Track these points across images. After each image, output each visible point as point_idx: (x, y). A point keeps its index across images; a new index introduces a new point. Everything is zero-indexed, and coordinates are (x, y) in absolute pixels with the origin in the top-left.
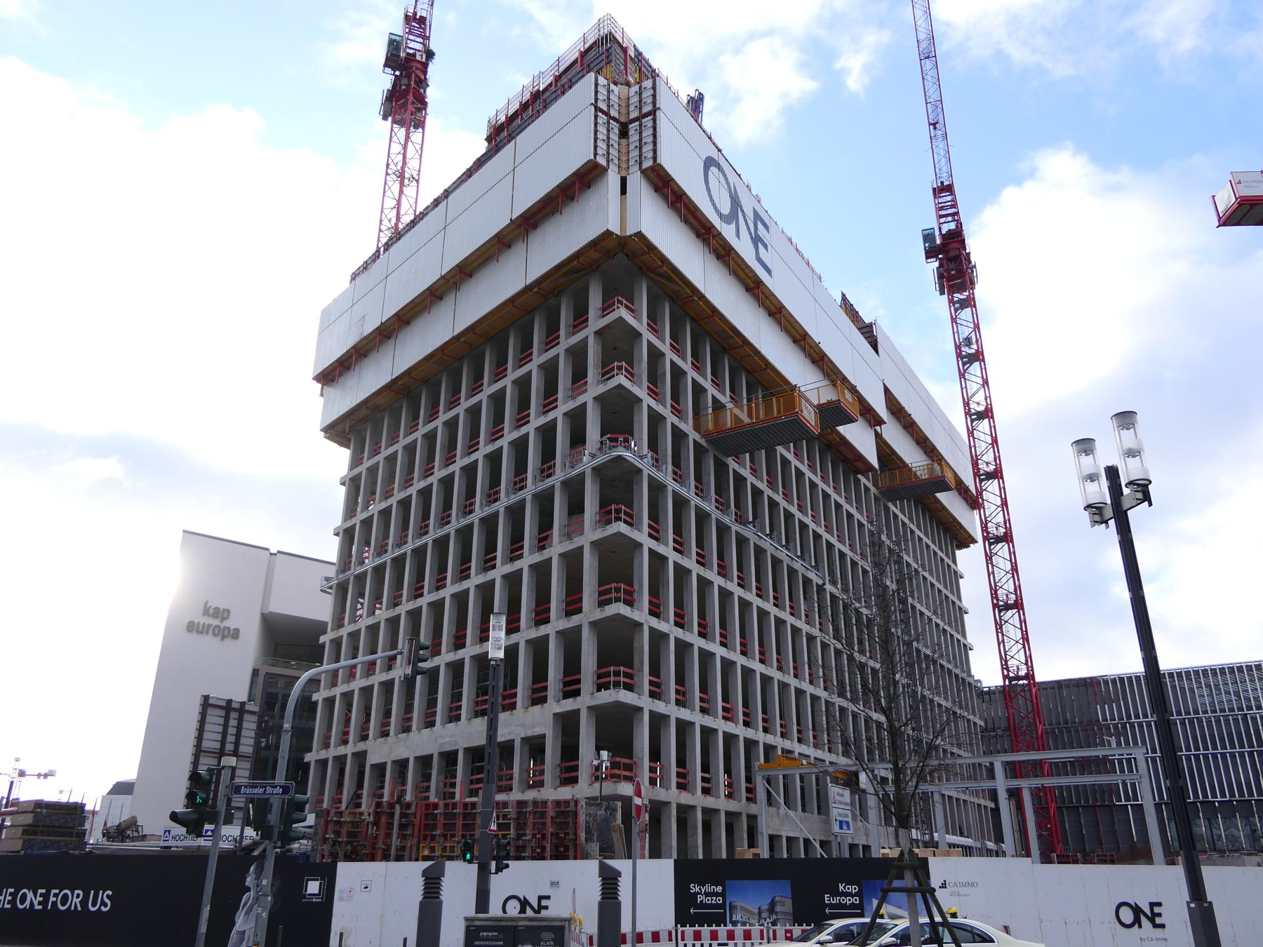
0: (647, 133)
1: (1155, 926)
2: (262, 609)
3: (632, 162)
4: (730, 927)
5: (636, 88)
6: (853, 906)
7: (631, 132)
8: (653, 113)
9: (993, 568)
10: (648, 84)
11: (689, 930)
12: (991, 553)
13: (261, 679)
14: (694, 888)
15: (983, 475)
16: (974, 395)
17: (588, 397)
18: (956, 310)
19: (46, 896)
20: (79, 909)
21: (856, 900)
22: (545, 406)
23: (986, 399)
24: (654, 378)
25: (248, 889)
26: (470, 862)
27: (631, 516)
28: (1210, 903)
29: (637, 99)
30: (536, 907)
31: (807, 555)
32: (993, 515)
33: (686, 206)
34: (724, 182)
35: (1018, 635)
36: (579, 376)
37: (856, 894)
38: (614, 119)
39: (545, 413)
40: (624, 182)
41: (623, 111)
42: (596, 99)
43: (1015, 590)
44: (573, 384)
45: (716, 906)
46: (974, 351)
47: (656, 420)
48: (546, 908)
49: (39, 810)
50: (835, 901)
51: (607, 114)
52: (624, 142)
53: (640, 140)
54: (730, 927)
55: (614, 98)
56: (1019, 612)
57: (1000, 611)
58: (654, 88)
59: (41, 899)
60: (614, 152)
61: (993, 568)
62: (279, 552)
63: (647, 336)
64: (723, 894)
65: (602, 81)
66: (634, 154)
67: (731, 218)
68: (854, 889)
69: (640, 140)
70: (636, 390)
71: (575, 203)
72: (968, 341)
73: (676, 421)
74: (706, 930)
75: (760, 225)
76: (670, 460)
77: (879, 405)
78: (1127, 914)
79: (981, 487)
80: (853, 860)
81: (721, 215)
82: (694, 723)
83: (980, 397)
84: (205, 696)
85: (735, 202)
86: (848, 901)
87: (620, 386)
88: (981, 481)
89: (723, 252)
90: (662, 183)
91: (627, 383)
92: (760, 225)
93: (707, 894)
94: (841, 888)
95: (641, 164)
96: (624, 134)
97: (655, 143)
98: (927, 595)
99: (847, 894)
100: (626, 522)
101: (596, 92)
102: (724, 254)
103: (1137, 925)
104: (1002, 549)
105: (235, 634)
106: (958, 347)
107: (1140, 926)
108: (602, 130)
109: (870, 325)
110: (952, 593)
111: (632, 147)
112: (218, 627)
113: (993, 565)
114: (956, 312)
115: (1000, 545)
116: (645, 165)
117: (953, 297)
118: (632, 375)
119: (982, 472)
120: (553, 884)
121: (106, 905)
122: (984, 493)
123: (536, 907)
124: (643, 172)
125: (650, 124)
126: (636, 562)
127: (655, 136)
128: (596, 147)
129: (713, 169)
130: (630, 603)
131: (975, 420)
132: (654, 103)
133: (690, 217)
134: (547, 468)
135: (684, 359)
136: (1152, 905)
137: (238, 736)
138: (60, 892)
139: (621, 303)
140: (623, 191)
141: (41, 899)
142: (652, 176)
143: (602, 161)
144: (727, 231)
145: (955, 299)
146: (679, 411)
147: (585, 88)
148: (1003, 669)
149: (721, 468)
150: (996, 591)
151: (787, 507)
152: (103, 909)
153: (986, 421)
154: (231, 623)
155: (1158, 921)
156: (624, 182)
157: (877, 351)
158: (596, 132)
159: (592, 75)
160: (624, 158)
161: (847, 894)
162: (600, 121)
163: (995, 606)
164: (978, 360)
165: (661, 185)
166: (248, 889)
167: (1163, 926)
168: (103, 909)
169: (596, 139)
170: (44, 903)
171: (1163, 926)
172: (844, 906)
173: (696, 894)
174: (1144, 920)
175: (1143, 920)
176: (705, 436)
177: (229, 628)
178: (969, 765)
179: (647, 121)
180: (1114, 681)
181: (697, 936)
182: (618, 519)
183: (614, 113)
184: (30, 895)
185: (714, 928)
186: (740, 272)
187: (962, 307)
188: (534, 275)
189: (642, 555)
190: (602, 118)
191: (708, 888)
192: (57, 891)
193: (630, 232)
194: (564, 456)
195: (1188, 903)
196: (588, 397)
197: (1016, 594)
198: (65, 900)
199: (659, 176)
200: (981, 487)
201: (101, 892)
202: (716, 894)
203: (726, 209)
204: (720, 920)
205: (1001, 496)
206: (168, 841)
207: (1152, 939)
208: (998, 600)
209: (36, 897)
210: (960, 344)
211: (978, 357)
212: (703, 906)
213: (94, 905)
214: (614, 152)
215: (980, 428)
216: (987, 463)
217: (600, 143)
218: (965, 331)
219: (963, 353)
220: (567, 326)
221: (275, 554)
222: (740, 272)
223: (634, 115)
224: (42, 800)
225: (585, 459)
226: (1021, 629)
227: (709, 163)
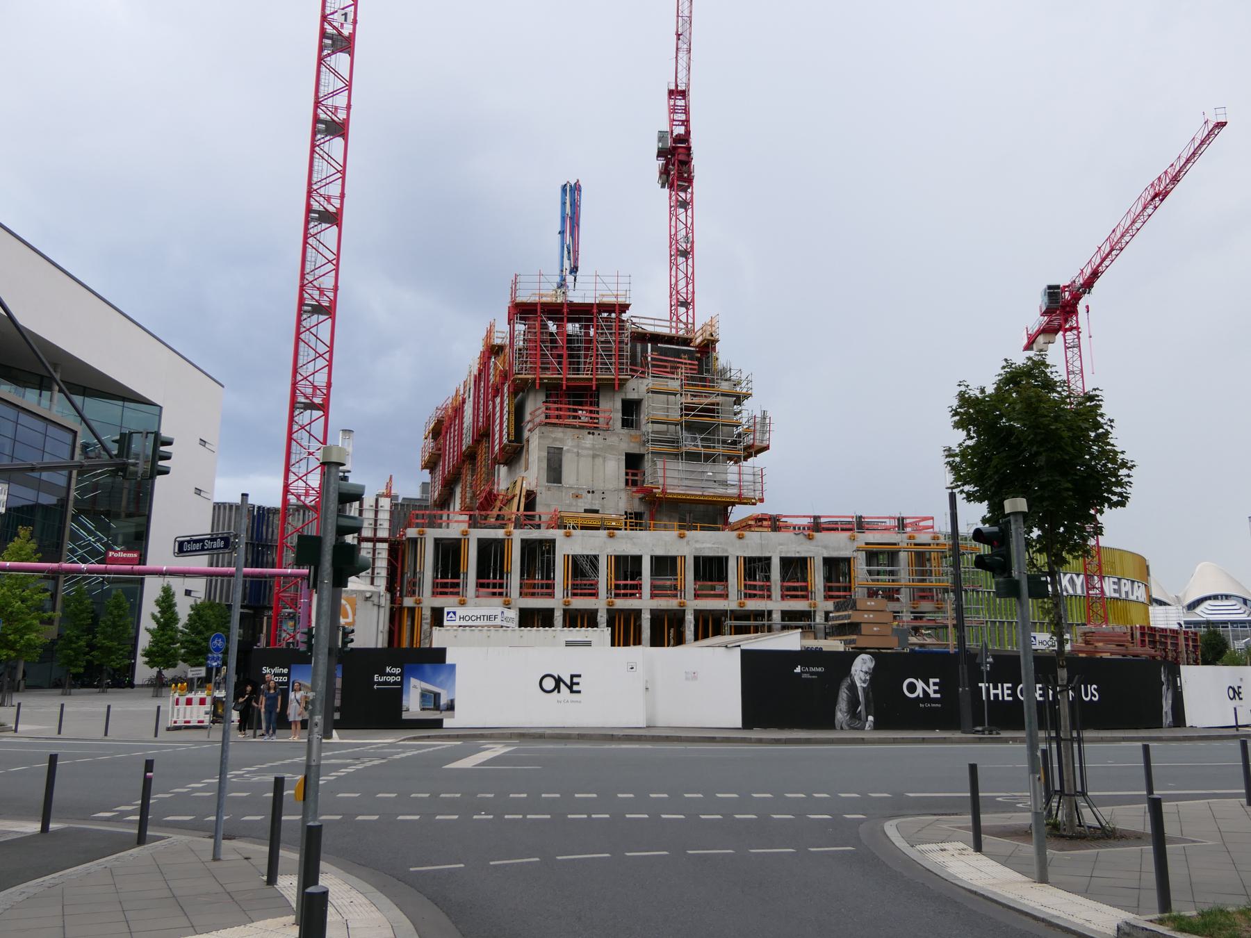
1: (572, 692)
21: (398, 679)
30: (569, 683)
37: (399, 675)
45: (395, 683)
48: (578, 684)
50: (383, 679)
59: (1041, 692)
68: (397, 671)
78: (549, 684)
80: (288, 650)
86: (391, 679)
93: (276, 675)
94: (388, 670)
99: (391, 675)
103: (556, 691)
107: (559, 692)
121: (1095, 697)
123: (569, 683)
141: (1041, 692)
152: (1093, 698)
155: (575, 688)
161: (391, 675)
178: (568, 556)
184: (920, 685)
191: (277, 670)
202: (283, 675)
206: (455, 620)
207: (568, 701)
209: (929, 687)
213: (1087, 696)
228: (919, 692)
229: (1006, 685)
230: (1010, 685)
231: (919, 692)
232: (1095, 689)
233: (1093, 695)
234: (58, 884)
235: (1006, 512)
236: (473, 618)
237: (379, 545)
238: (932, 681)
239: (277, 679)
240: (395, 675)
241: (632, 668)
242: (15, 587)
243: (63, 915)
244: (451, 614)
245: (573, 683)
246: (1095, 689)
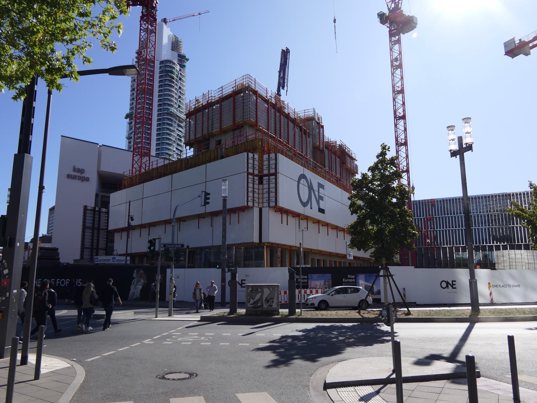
1: (453, 288)
2: (97, 170)
6: (353, 282)
9: (397, 129)
12: (398, 150)
13: (100, 198)
15: (398, 117)
16: (397, 83)
20: (66, 285)
21: (354, 280)
25: (135, 278)
26: (218, 268)
28: (476, 280)
32: (401, 134)
35: (404, 155)
37: (354, 278)
43: (407, 165)
48: (455, 285)
49: (41, 251)
50: (347, 280)
56: (407, 174)
61: (397, 129)
62: (103, 145)
68: (353, 277)
72: (396, 60)
78: (444, 285)
79: (395, 97)
84: (85, 206)
86: (351, 281)
88: (395, 94)
94: (349, 276)
105: (87, 179)
106: (392, 62)
107: (448, 288)
112: (80, 176)
113: (397, 128)
115: (402, 147)
117: (391, 39)
119: (397, 116)
120: (246, 276)
121: (80, 284)
122: (396, 99)
123: (451, 284)
131: (396, 94)
136: (453, 281)
137: (99, 221)
138: (60, 280)
145: (392, 40)
148: (396, 141)
150: (397, 138)
152: (79, 285)
154: (85, 175)
155: (454, 286)
166: (135, 278)
167: (455, 288)
168: (79, 285)
171: (455, 288)
172: (350, 282)
174: (449, 286)
175: (449, 285)
177: (84, 177)
180: (440, 201)
185: (305, 289)
187: (397, 69)
192: (59, 280)
195: (469, 280)
198: (63, 282)
200: (397, 123)
201: (77, 280)
202: (305, 279)
205: (406, 153)
210: (393, 60)
211: (400, 66)
216: (398, 87)
218: (395, 55)
219: (394, 65)
221: (101, 146)
224: (55, 248)
229: (39, 280)
230: (41, 279)
232: (80, 281)
236: (121, 261)
237: (271, 177)
239: (302, 281)
240: (352, 279)
241: (178, 277)
244: (114, 259)
245: (242, 283)
246: (80, 281)
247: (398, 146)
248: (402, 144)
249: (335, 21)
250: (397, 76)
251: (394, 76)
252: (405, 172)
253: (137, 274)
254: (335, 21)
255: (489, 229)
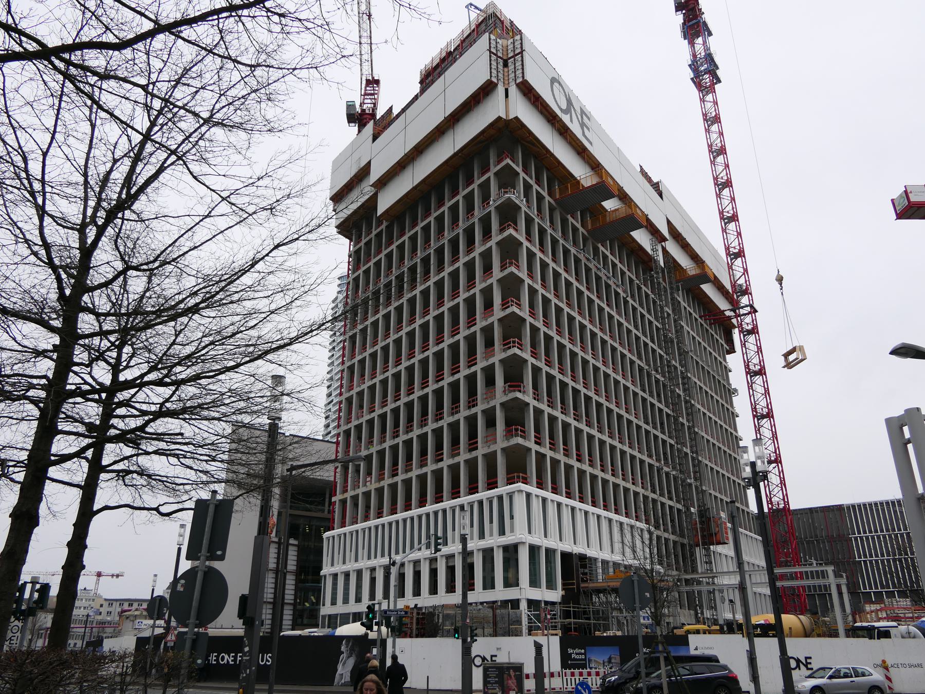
0: (519, 64)
3: (511, 80)
4: (589, 670)
5: (511, 40)
7: (510, 64)
8: (521, 53)
10: (518, 37)
11: (568, 671)
14: (570, 651)
17: (493, 280)
18: (725, 224)
19: (235, 657)
22: (468, 323)
23: (739, 244)
24: (527, 195)
27: (521, 345)
29: (512, 46)
31: (615, 275)
33: (542, 104)
34: (561, 89)
36: (488, 269)
38: (500, 57)
39: (468, 291)
40: (507, 91)
41: (505, 53)
42: (490, 47)
44: (484, 273)
45: (581, 660)
46: (737, 251)
47: (536, 370)
48: (810, 663)
51: (496, 55)
52: (506, 70)
53: (515, 68)
54: (589, 670)
55: (499, 47)
57: (758, 420)
58: (521, 39)
60: (501, 75)
63: (528, 281)
64: (585, 654)
65: (493, 37)
66: (512, 75)
67: (567, 111)
69: (515, 68)
70: (520, 275)
71: (480, 104)
73: (546, 330)
74: (577, 671)
75: (584, 117)
76: (545, 394)
77: (665, 231)
81: (561, 109)
82: (560, 461)
83: (735, 244)
85: (569, 102)
87: (513, 312)
89: (563, 131)
90: (527, 90)
91: (517, 311)
92: (584, 117)
93: (577, 654)
95: (515, 80)
96: (506, 65)
97: (523, 69)
98: (715, 456)
100: (518, 348)
101: (490, 43)
102: (563, 131)
104: (758, 380)
107: (800, 669)
108: (494, 63)
109: (658, 183)
110: (730, 426)
111: (510, 72)
114: (725, 225)
115: (765, 420)
116: (518, 81)
118: (518, 267)
120: (498, 649)
123: (804, 662)
124: (518, 85)
125: (520, 59)
126: (528, 459)
127: (523, 65)
128: (491, 72)
129: (556, 84)
130: (523, 437)
132: (522, 47)
133: (544, 110)
134: (471, 321)
135: (543, 189)
136: (806, 658)
139: (513, 301)
140: (507, 96)
142: (522, 86)
143: (495, 80)
144: (565, 119)
146: (545, 287)
147: (483, 42)
148: (753, 411)
149: (564, 222)
151: (615, 377)
153: (740, 259)
155: (809, 666)
156: (507, 91)
157: (662, 198)
158: (491, 64)
159: (487, 34)
160: (506, 78)
162: (492, 59)
163: (754, 416)
164: (740, 256)
165: (527, 91)
166: (343, 653)
169: (491, 68)
170: (235, 660)
173: (571, 654)
175: (801, 664)
176: (555, 200)
179: (518, 57)
181: (573, 674)
182: (517, 435)
183: (500, 54)
184: (226, 657)
186: (574, 143)
188: (459, 146)
189: (531, 455)
190: (494, 57)
191: (577, 651)
193: (511, 117)
194: (482, 394)
196: (493, 280)
197: (768, 408)
199: (525, 87)
202: (581, 654)
203: (564, 107)
204: (584, 666)
208: (756, 412)
212: (575, 659)
213: (262, 661)
214: (501, 75)
215: (736, 263)
217: (493, 71)
220: (481, 314)
222: (574, 143)
223: (511, 55)
225: (491, 203)
226: (780, 476)
227: (553, 81)
228: (225, 661)
231: (225, 661)
233: (267, 660)
234: (309, 232)
235: (783, 616)
238: (232, 655)
242: (160, 366)
243: (222, 232)
247: (758, 420)
248: (763, 417)
249: (780, 280)
250: (737, 268)
251: (733, 270)
252: (177, 156)
253: (347, 647)
254: (780, 280)
255: (877, 561)
